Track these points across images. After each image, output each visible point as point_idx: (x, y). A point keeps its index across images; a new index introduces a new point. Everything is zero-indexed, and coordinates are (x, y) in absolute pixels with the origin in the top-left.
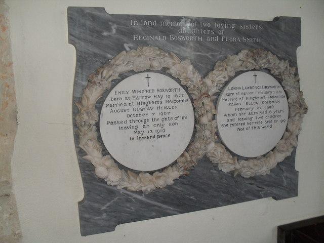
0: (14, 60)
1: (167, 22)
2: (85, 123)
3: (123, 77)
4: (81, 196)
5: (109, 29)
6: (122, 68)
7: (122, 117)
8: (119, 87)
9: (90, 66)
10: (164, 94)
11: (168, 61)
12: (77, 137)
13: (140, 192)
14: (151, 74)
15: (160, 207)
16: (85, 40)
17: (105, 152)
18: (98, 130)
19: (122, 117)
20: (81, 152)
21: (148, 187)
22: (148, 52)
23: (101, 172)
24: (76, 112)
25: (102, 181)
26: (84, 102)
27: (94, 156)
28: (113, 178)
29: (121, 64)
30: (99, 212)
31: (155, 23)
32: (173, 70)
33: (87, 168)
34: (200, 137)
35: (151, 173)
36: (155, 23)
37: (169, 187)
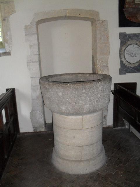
0: (110, 42)
1: (137, 35)
2: (122, 53)
3: (129, 45)
4: (120, 67)
5: (126, 36)
6: (129, 44)
7: (129, 52)
8: (128, 47)
9: (123, 44)
10: (136, 49)
11: (137, 42)
12: (120, 56)
13: (131, 67)
14: (134, 45)
15: (9, 111)
16: (122, 38)
17: (125, 59)
18: (124, 55)
19: (129, 52)
20: (121, 59)
21: (132, 66)
22: (134, 41)
23: (124, 62)
24: (120, 51)
25: (124, 64)
26: (122, 49)
27: (123, 59)
28: (126, 64)
29: (129, 43)
30: (123, 70)
31: (135, 35)
32: (138, 44)
33: (122, 62)
34: (37, 62)
35: (133, 63)
36: (135, 35)
37: (136, 67)
